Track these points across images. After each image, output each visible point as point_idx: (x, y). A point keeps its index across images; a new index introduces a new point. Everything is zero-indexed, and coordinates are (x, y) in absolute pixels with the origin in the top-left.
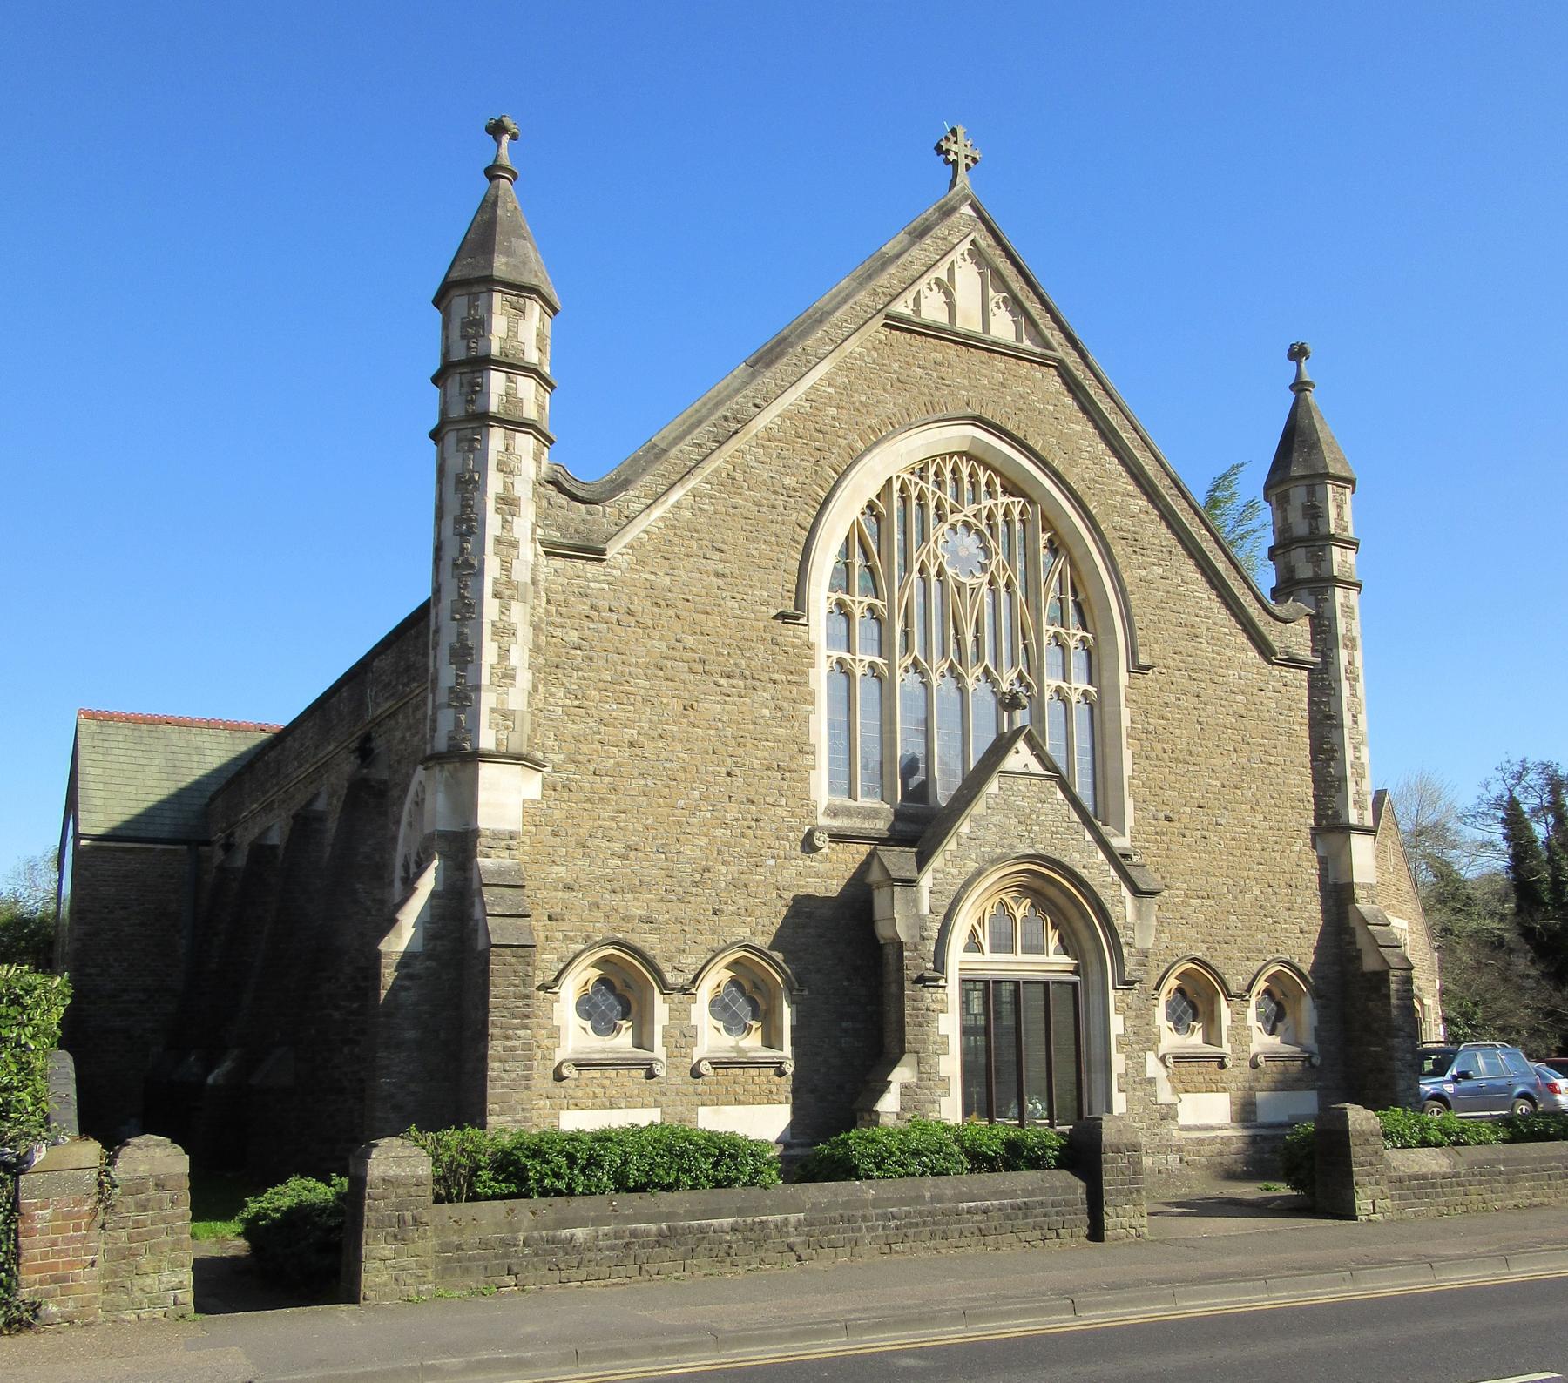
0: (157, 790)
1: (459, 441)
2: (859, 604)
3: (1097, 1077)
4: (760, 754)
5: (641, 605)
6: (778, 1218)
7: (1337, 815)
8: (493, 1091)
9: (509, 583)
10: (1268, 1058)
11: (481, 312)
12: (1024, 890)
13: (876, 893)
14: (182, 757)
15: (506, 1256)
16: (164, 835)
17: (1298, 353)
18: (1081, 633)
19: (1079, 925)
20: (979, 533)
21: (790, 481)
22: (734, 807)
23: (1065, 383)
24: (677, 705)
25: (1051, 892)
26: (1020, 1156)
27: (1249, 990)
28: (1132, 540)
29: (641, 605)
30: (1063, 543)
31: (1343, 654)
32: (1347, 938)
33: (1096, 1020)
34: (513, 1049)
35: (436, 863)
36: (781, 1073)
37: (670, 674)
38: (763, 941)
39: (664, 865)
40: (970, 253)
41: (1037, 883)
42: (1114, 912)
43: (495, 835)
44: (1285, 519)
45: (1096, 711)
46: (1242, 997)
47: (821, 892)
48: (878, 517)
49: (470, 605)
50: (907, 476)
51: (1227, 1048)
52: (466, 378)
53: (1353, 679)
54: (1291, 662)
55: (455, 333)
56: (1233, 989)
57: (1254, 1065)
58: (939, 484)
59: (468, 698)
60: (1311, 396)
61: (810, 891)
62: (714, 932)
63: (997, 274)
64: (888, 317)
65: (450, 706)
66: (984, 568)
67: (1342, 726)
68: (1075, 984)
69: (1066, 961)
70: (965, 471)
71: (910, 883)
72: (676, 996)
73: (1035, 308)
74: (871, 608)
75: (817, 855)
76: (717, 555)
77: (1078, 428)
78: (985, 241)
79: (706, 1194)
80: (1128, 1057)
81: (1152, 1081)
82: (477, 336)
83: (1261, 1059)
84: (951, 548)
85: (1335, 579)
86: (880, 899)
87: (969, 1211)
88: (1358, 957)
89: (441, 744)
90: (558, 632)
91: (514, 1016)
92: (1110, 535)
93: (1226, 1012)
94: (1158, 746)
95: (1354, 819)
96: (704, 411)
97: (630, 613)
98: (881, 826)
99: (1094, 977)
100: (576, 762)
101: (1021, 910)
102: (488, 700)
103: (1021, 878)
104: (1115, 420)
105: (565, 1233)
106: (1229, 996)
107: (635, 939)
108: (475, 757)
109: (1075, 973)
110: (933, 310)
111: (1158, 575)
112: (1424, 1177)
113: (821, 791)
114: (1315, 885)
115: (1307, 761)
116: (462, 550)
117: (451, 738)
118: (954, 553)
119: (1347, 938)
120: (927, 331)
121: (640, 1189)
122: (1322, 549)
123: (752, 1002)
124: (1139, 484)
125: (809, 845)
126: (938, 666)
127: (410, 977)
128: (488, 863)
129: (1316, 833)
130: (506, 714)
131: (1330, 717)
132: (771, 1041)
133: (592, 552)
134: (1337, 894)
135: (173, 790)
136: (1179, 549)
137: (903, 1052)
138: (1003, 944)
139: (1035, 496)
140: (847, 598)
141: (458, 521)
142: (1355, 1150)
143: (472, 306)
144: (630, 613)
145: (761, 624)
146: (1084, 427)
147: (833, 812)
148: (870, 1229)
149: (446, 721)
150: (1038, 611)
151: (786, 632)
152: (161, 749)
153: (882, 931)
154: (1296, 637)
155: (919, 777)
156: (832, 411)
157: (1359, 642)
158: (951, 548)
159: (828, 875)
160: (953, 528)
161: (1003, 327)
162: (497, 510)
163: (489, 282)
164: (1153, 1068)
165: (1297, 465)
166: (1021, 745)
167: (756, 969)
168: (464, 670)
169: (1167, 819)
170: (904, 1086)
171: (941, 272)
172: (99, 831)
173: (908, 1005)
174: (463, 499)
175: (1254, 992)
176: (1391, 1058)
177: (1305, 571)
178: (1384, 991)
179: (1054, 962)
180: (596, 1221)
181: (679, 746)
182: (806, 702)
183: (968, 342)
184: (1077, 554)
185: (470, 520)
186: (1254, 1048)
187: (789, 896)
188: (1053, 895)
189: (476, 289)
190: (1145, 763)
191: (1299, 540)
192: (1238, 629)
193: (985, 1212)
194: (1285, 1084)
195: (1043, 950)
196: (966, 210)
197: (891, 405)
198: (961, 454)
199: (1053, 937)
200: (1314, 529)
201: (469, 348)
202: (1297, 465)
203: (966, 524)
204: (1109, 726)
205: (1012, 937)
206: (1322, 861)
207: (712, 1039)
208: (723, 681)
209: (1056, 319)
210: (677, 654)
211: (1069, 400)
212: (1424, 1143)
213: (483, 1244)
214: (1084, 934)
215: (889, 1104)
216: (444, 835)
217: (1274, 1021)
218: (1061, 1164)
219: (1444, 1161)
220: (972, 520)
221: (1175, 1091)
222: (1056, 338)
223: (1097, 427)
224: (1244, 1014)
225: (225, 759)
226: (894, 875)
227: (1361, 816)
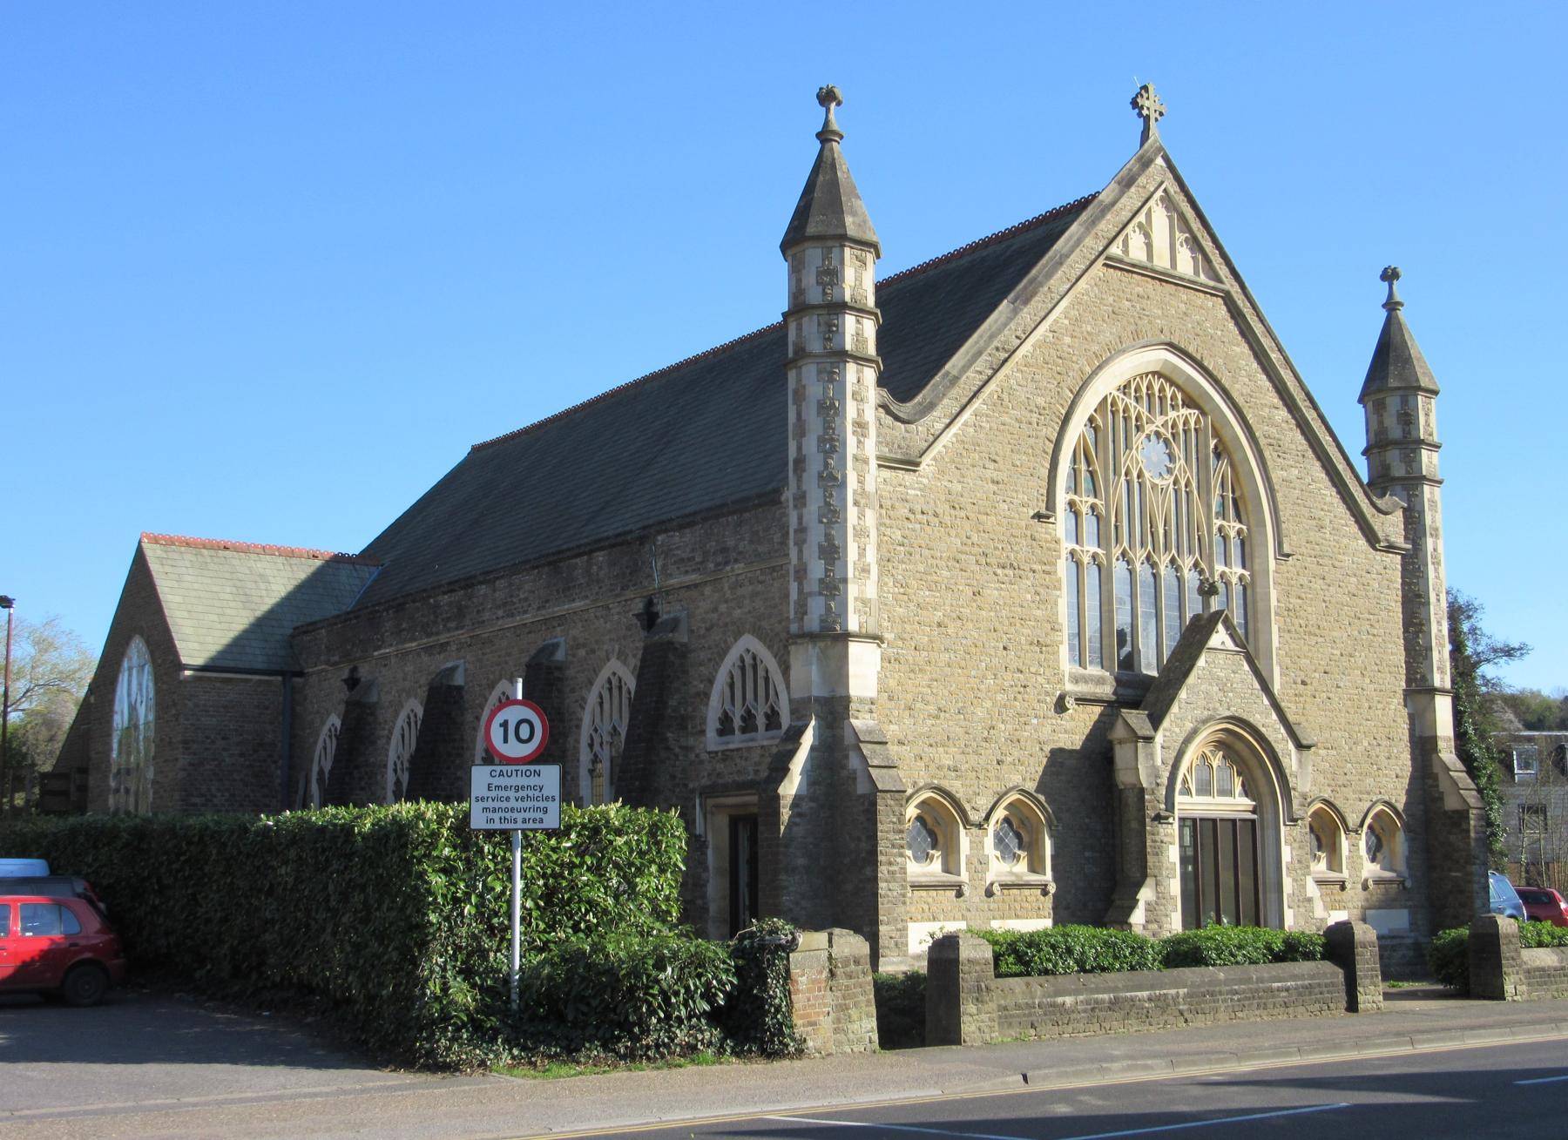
0: (240, 621)
1: (819, 372)
2: (1085, 502)
3: (1272, 897)
4: (1027, 631)
5: (943, 508)
6: (1173, 992)
7: (1424, 678)
8: (883, 906)
9: (864, 493)
10: (1376, 882)
12: (1220, 745)
13: (1117, 748)
14: (250, 585)
15: (1030, 1015)
16: (260, 666)
17: (1390, 275)
18: (1238, 526)
19: (1258, 773)
20: (1166, 441)
21: (1040, 401)
22: (1008, 676)
23: (1229, 311)
24: (969, 591)
25: (1239, 746)
26: (1297, 951)
27: (987, 818)
28: (1277, 446)
29: (943, 508)
30: (1226, 449)
31: (1430, 541)
32: (1430, 782)
33: (1270, 852)
34: (894, 873)
35: (813, 723)
36: (1045, 893)
37: (963, 565)
38: (1031, 786)
39: (963, 723)
40: (1162, 199)
41: (1230, 740)
42: (1285, 761)
43: (861, 701)
44: (1381, 423)
45: (1249, 592)
46: (1356, 832)
47: (1068, 746)
48: (1096, 429)
49: (835, 512)
50: (1116, 393)
51: (1345, 874)
53: (1437, 564)
54: (1391, 548)
55: (810, 279)
56: (1351, 825)
57: (1365, 887)
58: (1137, 399)
60: (1402, 314)
61: (1061, 745)
62: (998, 778)
63: (1182, 217)
64: (1108, 258)
65: (820, 594)
66: (1170, 471)
67: (1429, 603)
68: (1253, 821)
69: (1247, 803)
70: (1156, 388)
71: (1149, 740)
72: (974, 830)
73: (1208, 245)
74: (1093, 507)
75: (1066, 715)
76: (992, 465)
77: (1238, 350)
78: (1173, 188)
79: (1126, 974)
80: (1295, 880)
81: (1310, 900)
82: (832, 284)
83: (1370, 883)
84: (1145, 455)
85: (1424, 478)
86: (1121, 754)
87: (1279, 989)
88: (1441, 798)
89: (813, 622)
90: (888, 532)
91: (893, 846)
92: (1262, 442)
93: (965, 839)
94: (1296, 622)
95: (1437, 684)
96: (982, 342)
97: (936, 515)
98: (1107, 690)
99: (1269, 816)
100: (903, 640)
101: (1217, 761)
102: (853, 591)
103: (1220, 735)
104: (1266, 342)
105: (1060, 1000)
106: (1347, 830)
107: (946, 784)
108: (846, 637)
109: (1254, 812)
110: (1137, 253)
111: (1297, 479)
112: (1543, 969)
113: (1067, 665)
114: (1406, 737)
116: (826, 465)
117: (822, 621)
118: (1148, 458)
119: (1430, 782)
120: (1132, 269)
121: (1092, 971)
123: (1018, 835)
124: (1282, 398)
125: (1060, 706)
126: (1139, 555)
127: (800, 815)
128: (860, 722)
129: (1408, 694)
130: (865, 602)
131: (1419, 596)
132: (1035, 867)
133: (910, 464)
134: (1423, 745)
135: (252, 620)
136: (1310, 453)
137: (1144, 876)
138: (1205, 789)
139: (1206, 409)
140: (1076, 498)
141: (821, 440)
142: (1503, 948)
143: (826, 256)
144: (936, 515)
145: (1023, 523)
146: (1244, 349)
147: (1076, 680)
148: (1225, 1001)
149: (816, 607)
150: (1209, 506)
151: (1040, 528)
152: (227, 575)
153: (1123, 778)
154: (1392, 527)
155: (1127, 649)
156: (1068, 340)
157: (1441, 532)
158: (1145, 455)
159: (1074, 730)
160: (1148, 437)
161: (1186, 264)
162: (854, 433)
163: (843, 238)
164: (1312, 890)
165: (1390, 374)
166: (1220, 627)
167: (1024, 810)
168: (833, 564)
169: (1304, 683)
170: (1148, 904)
171: (1141, 218)
172: (200, 661)
173: (1149, 837)
174: (825, 422)
175: (993, 820)
176: (1470, 882)
177: (1398, 470)
178: (1464, 826)
179: (1237, 804)
180: (1076, 992)
181: (970, 625)
182: (1055, 588)
183: (1162, 278)
184: (1237, 457)
185: (832, 440)
186: (1365, 874)
187: (1047, 749)
188: (1243, 751)
189: (830, 243)
190: (1287, 636)
191: (1395, 443)
192: (1351, 521)
193: (1287, 990)
194: (1386, 903)
195: (1230, 793)
196: (1159, 161)
197: (1108, 334)
198: (1154, 373)
199: (1238, 781)
200: (1407, 433)
201: (825, 294)
202: (1390, 374)
203: (1158, 434)
204: (1260, 605)
205: (1209, 783)
206: (1411, 717)
207: (999, 869)
208: (999, 571)
209: (1224, 256)
210: (967, 549)
211: (1231, 325)
212: (1540, 945)
213: (1017, 1006)
214: (1262, 781)
215: (1138, 917)
216: (817, 699)
217: (1376, 850)
218: (1323, 958)
219: (1555, 958)
220: (1162, 430)
221: (1326, 908)
222: (1223, 271)
223: (1252, 348)
224: (982, 842)
225: (290, 588)
226: (1140, 733)
227: (1442, 680)
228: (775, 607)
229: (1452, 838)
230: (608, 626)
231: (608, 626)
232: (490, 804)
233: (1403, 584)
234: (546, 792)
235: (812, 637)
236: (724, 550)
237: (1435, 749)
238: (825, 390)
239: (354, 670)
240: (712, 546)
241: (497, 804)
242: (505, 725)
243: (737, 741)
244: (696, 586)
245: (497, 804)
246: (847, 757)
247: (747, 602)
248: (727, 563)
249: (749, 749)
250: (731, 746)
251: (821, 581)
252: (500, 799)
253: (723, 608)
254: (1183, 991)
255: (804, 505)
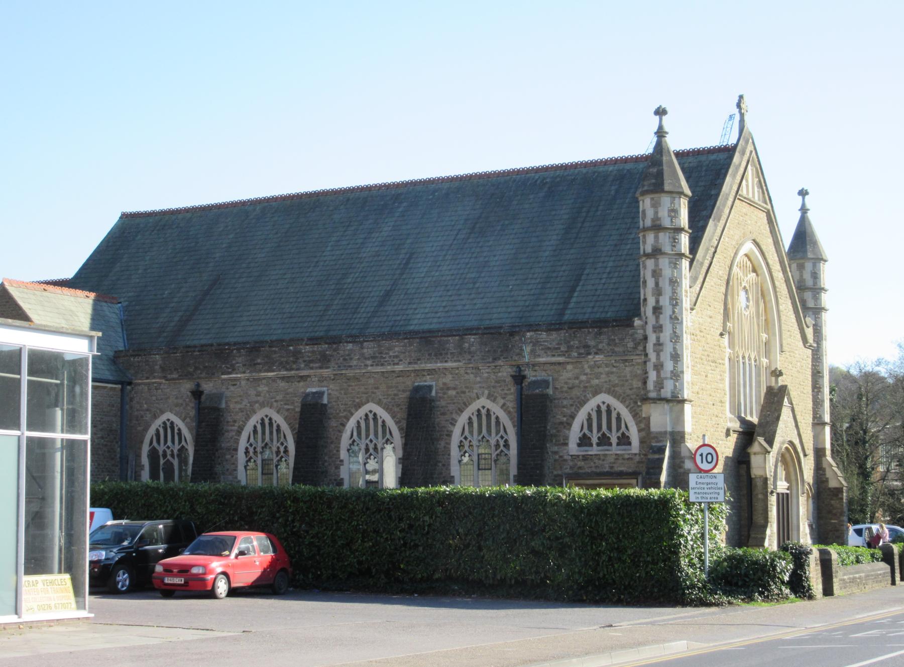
1: (670, 263)
3: (795, 533)
5: (698, 333)
7: (820, 417)
11: (677, 206)
17: (660, 112)
29: (698, 333)
44: (801, 276)
52: (672, 235)
59: (679, 376)
60: (810, 215)
68: (787, 494)
82: (675, 217)
88: (827, 481)
89: (667, 392)
99: (794, 492)
108: (683, 401)
115: (810, 391)
116: (674, 312)
117: (673, 393)
122: (818, 293)
129: (814, 425)
131: (819, 372)
139: (759, 272)
141: (671, 299)
149: (669, 386)
153: (756, 472)
177: (811, 304)
189: (674, 195)
200: (815, 283)
201: (672, 222)
206: (814, 437)
215: (766, 544)
228: (627, 381)
229: (833, 502)
230: (478, 379)
231: (478, 379)
232: (697, 491)
233: (813, 365)
234: (719, 486)
235: (667, 401)
236: (587, 346)
237: (824, 455)
238: (673, 272)
239: (198, 385)
240: (575, 343)
241: (700, 491)
242: (701, 455)
243: (595, 450)
244: (559, 364)
245: (700, 491)
246: (683, 462)
247: (603, 376)
248: (589, 354)
249: (605, 455)
250: (590, 453)
251: (672, 372)
252: (701, 488)
253: (583, 378)
254: (863, 575)
255: (662, 331)
